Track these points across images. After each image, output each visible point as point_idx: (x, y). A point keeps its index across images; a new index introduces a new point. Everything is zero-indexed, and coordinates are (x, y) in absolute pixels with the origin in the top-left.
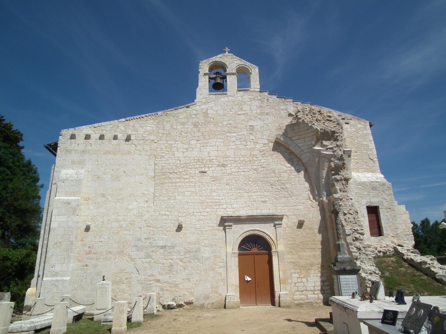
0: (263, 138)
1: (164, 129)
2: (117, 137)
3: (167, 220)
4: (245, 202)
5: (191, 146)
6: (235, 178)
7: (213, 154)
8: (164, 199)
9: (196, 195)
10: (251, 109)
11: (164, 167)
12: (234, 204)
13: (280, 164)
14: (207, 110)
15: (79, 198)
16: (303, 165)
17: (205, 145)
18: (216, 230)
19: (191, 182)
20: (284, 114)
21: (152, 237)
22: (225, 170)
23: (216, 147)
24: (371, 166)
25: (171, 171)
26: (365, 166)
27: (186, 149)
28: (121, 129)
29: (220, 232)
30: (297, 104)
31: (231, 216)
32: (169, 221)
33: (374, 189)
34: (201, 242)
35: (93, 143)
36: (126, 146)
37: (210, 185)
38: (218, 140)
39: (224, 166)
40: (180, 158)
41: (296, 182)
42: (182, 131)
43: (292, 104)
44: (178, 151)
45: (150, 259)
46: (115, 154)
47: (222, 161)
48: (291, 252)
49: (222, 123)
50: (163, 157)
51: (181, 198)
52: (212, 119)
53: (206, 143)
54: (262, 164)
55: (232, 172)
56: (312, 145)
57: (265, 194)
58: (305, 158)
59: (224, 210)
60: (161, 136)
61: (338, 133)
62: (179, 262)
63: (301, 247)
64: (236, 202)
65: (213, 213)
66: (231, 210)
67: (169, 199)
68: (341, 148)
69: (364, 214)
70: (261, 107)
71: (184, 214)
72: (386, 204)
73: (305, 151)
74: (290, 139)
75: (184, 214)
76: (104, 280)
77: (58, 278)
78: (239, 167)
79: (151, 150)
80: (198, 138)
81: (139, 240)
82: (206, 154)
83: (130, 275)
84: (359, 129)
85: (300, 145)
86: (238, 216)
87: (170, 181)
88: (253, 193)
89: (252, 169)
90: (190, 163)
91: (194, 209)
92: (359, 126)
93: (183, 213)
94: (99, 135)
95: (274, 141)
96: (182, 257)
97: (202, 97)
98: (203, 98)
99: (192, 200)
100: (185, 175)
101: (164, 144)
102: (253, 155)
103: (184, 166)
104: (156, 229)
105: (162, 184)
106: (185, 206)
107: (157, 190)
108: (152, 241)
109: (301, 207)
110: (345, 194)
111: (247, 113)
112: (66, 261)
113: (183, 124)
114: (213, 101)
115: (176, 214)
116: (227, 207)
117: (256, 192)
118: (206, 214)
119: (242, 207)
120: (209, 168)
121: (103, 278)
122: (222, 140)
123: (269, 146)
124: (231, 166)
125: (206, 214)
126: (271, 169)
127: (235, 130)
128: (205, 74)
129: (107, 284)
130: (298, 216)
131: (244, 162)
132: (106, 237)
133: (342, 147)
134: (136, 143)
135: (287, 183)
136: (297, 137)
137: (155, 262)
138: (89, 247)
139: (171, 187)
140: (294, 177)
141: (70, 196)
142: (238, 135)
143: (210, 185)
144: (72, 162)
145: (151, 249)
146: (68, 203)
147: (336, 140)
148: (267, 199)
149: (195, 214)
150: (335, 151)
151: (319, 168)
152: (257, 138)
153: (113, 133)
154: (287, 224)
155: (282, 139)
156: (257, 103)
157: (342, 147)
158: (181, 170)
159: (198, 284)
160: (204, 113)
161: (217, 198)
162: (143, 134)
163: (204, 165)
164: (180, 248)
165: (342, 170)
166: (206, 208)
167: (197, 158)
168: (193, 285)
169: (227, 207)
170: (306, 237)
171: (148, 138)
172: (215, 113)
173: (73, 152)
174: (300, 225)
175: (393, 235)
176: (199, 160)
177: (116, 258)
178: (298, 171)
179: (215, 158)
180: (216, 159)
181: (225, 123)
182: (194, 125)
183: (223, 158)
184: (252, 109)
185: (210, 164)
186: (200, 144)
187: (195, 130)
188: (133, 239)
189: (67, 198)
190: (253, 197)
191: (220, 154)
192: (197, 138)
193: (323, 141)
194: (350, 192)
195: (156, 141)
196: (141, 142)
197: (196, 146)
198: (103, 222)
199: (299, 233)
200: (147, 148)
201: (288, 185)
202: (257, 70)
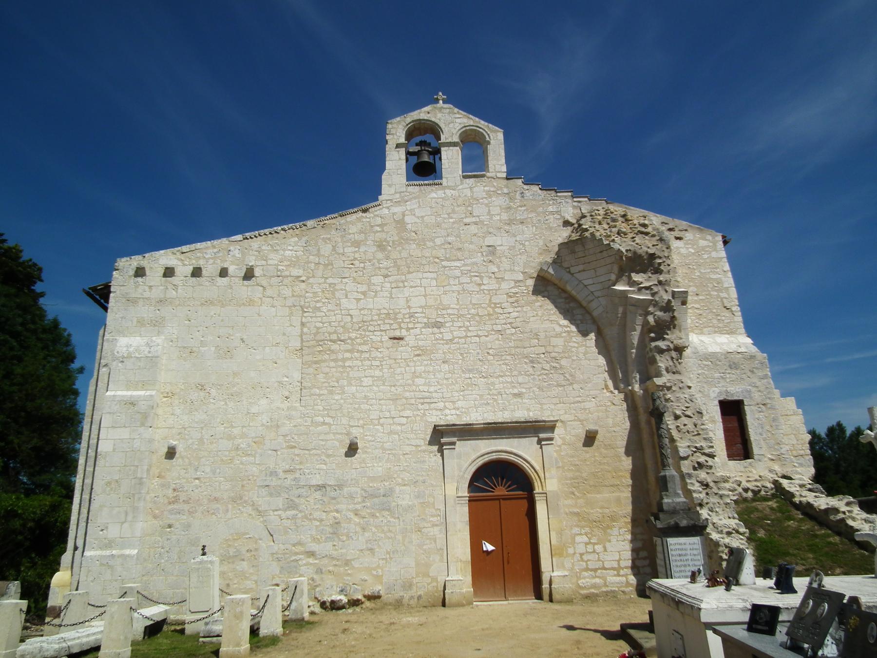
1: (318, 255)
4: (481, 396)
5: (372, 287)
7: (417, 302)
8: (322, 392)
9: (384, 385)
12: (459, 400)
13: (547, 319)
14: (404, 215)
15: (154, 393)
17: (401, 285)
19: (374, 359)
20: (555, 222)
21: (298, 467)
22: (441, 333)
25: (334, 337)
26: (715, 321)
27: (364, 293)
28: (234, 256)
30: (579, 202)
31: (454, 425)
32: (331, 436)
33: (734, 366)
34: (395, 476)
36: (244, 290)
37: (411, 364)
38: (425, 275)
39: (438, 325)
40: (351, 312)
41: (581, 356)
42: (355, 259)
43: (570, 201)
44: (346, 297)
46: (223, 306)
48: (573, 493)
50: (319, 309)
51: (354, 391)
52: (413, 234)
53: (403, 282)
54: (513, 321)
55: (454, 338)
57: (520, 379)
58: (598, 308)
59: (439, 413)
60: (313, 268)
61: (660, 258)
62: (352, 515)
63: (592, 483)
64: (463, 396)
65: (418, 418)
66: (454, 412)
67: (331, 393)
68: (667, 288)
70: (509, 208)
71: (361, 422)
72: (757, 396)
73: (597, 294)
76: (204, 554)
77: (114, 552)
78: (467, 327)
79: (293, 296)
81: (274, 473)
82: (402, 302)
83: (256, 543)
84: (703, 250)
85: (586, 282)
86: (467, 425)
87: (333, 357)
88: (497, 378)
89: (493, 330)
90: (372, 320)
92: (702, 243)
93: (358, 419)
94: (191, 268)
95: (535, 275)
97: (392, 191)
98: (396, 193)
99: (375, 393)
101: (320, 284)
103: (360, 328)
104: (307, 452)
105: (316, 363)
108: (297, 475)
109: (591, 405)
110: (677, 376)
111: (482, 222)
112: (130, 518)
113: (357, 244)
114: (415, 198)
115: (345, 421)
117: (502, 376)
118: (404, 420)
119: (476, 407)
120: (408, 329)
121: (203, 549)
122: (434, 275)
123: (525, 286)
126: (531, 332)
127: (459, 254)
129: (211, 562)
131: (477, 318)
132: (208, 469)
133: (669, 285)
135: (562, 358)
136: (581, 267)
137: (306, 517)
138: (174, 490)
139: (334, 370)
140: (576, 345)
141: (136, 389)
142: (464, 265)
143: (411, 364)
145: (297, 492)
146: (133, 404)
147: (658, 271)
148: (524, 390)
149: (382, 421)
150: (656, 293)
151: (624, 329)
154: (563, 439)
155: (551, 271)
156: (501, 201)
157: (669, 285)
158: (353, 335)
160: (397, 222)
161: (426, 388)
162: (278, 265)
163: (399, 324)
164: (353, 489)
165: (670, 330)
168: (381, 562)
170: (600, 463)
171: (287, 273)
173: (141, 303)
174: (590, 439)
176: (389, 314)
177: (227, 511)
179: (420, 310)
180: (422, 313)
181: (438, 241)
182: (379, 246)
183: (437, 309)
184: (492, 213)
185: (410, 322)
187: (380, 255)
188: (261, 471)
189: (129, 393)
190: (497, 387)
191: (431, 302)
193: (633, 275)
195: (304, 278)
196: (275, 280)
198: (201, 440)
199: (588, 455)
200: (287, 292)
201: (564, 362)
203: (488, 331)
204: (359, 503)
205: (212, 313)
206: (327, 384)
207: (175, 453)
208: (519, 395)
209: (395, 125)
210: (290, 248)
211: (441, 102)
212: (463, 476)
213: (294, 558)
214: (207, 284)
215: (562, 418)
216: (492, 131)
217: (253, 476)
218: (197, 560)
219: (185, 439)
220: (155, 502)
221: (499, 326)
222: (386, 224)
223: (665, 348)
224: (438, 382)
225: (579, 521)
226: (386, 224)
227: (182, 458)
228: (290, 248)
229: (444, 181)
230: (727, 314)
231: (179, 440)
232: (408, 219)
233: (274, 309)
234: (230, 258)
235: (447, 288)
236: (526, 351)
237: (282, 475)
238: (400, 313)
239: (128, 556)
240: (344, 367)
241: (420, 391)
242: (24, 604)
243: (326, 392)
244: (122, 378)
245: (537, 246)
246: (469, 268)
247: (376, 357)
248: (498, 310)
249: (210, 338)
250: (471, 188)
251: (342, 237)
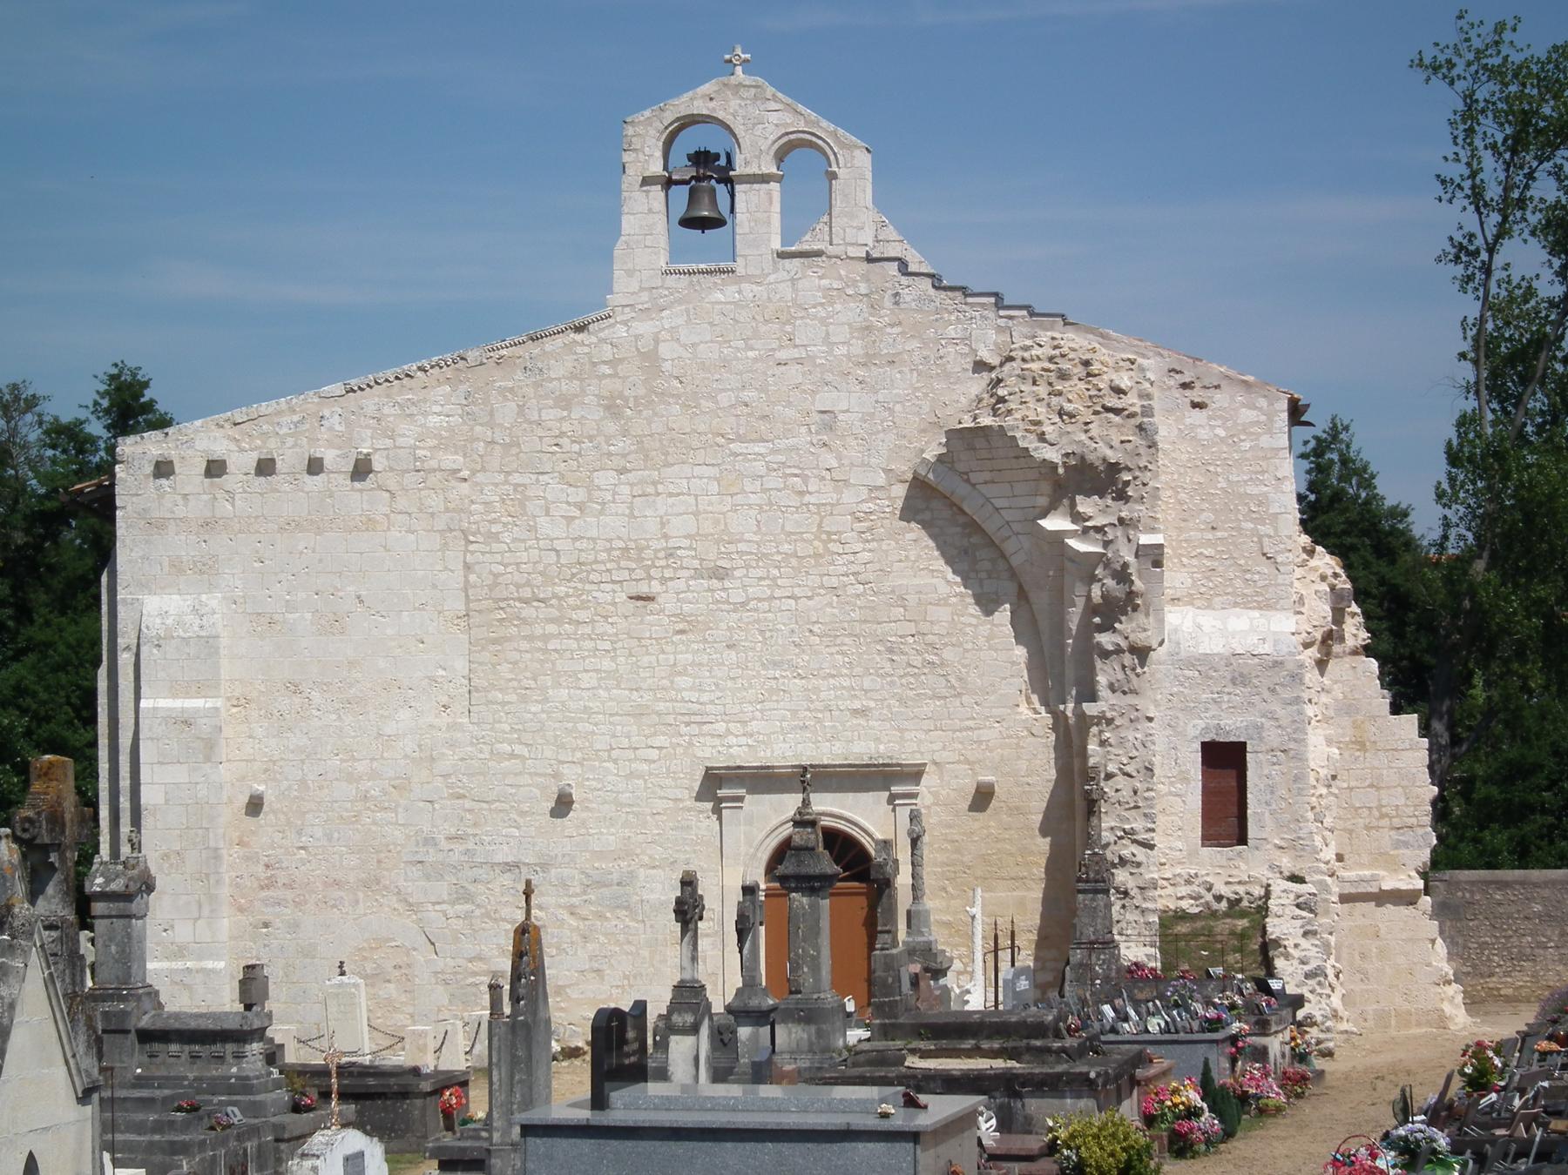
0: (868, 465)
1: (491, 425)
2: (322, 465)
3: (521, 773)
4: (794, 712)
5: (596, 494)
6: (758, 621)
7: (681, 526)
8: (507, 698)
9: (618, 686)
10: (826, 339)
11: (500, 580)
12: (754, 719)
13: (923, 570)
14: (657, 341)
15: (219, 703)
16: (1013, 574)
17: (651, 490)
18: (689, 810)
19: (601, 637)
20: (957, 361)
21: (470, 831)
22: (724, 589)
23: (691, 500)
24: (1260, 583)
25: (526, 593)
26: (1238, 583)
27: (580, 507)
28: (331, 429)
29: (702, 820)
30: (1011, 318)
31: (739, 767)
32: (526, 779)
33: (1240, 679)
34: (638, 851)
35: (238, 488)
36: (356, 498)
37: (669, 648)
38: (698, 471)
39: (719, 574)
40: (557, 545)
42: (562, 435)
43: (991, 315)
44: (547, 514)
45: (468, 907)
46: (319, 531)
47: (712, 556)
48: (944, 889)
49: (713, 398)
50: (495, 537)
51: (565, 697)
52: (676, 383)
53: (654, 483)
54: (861, 569)
55: (749, 600)
56: (1037, 511)
57: (867, 683)
58: (1018, 551)
59: (717, 742)
60: (481, 451)
61: (1130, 470)
62: (566, 916)
63: (979, 873)
64: (762, 711)
65: (680, 750)
66: (743, 740)
67: (524, 699)
69: (1188, 772)
70: (868, 328)
71: (579, 755)
72: (1273, 736)
73: (1015, 527)
74: (965, 477)
75: (579, 755)
76: (343, 974)
77: (189, 964)
78: (774, 579)
79: (447, 510)
80: (622, 462)
81: (430, 841)
82: (652, 526)
83: (408, 954)
84: (1244, 431)
85: (999, 503)
86: (762, 768)
87: (526, 631)
88: (824, 678)
89: (822, 586)
90: (596, 562)
91: (614, 736)
92: (1247, 415)
93: (574, 750)
94: (255, 456)
95: (909, 476)
96: (575, 900)
97: (635, 286)
98: (642, 289)
99: (603, 703)
100: (578, 608)
101: (496, 485)
102: (829, 533)
103: (574, 575)
104: (485, 806)
105: (495, 642)
106: (580, 726)
107: (480, 664)
108: (471, 846)
109: (990, 734)
110: (1130, 699)
111: (812, 358)
112: (206, 912)
113: (565, 402)
114: (680, 302)
115: (549, 752)
116: (728, 730)
117: (833, 676)
118: (654, 754)
119: (782, 731)
120: (663, 581)
121: (341, 967)
122: (713, 471)
123: (889, 498)
124: (746, 576)
125: (654, 754)
126: (893, 592)
127: (763, 427)
128: (647, 181)
129: (356, 986)
130: (977, 767)
131: (794, 562)
132: (319, 833)
134: (392, 482)
135: (946, 645)
136: (987, 476)
137: (487, 914)
138: (267, 866)
139: (529, 656)
141: (188, 696)
142: (774, 452)
143: (669, 648)
144: (172, 565)
145: (471, 874)
146: (186, 723)
147: (1122, 496)
148: (872, 704)
149: (614, 754)
152: (845, 462)
153: (308, 450)
154: (935, 795)
155: (931, 476)
156: (850, 312)
158: (561, 590)
159: (631, 986)
160: (643, 356)
161: (694, 696)
162: (416, 448)
163: (647, 569)
164: (566, 872)
165: (1126, 614)
166: (655, 734)
167: (621, 544)
168: (614, 991)
169: (728, 730)
170: (998, 840)
171: (433, 464)
172: (686, 355)
173: (172, 527)
174: (982, 798)
175: (1283, 844)
176: (627, 549)
177: (357, 902)
178: (987, 604)
179: (686, 543)
180: (690, 548)
181: (725, 399)
182: (607, 408)
183: (717, 542)
184: (833, 339)
185: (668, 566)
186: (632, 485)
187: (611, 427)
188: (408, 837)
189: (178, 703)
190: (823, 695)
191: (707, 527)
192: (618, 462)
193: (1078, 498)
194: (1150, 693)
195: (465, 473)
196: (410, 479)
197: (615, 493)
198: (303, 782)
199: (976, 825)
200: (435, 502)
201: (948, 654)
202: (864, 160)
203: (813, 589)
204: (577, 895)
205: (300, 548)
206: (515, 684)
207: (262, 805)
208: (862, 712)
209: (640, 129)
210: (436, 409)
211: (739, 70)
212: (755, 855)
213: (471, 980)
214: (286, 487)
215: (937, 758)
216: (843, 146)
217: (396, 845)
218: (334, 981)
219: (275, 780)
220: (237, 886)
221: (834, 579)
222: (621, 360)
223: (1111, 648)
224: (717, 685)
225: (951, 935)
226: (621, 360)
227: (274, 812)
228: (436, 409)
229: (740, 266)
230: (1266, 568)
231: (265, 782)
232: (665, 350)
233: (412, 537)
234: (324, 434)
235: (739, 499)
236: (879, 629)
237: (444, 845)
238: (648, 547)
239: (213, 971)
240: (545, 651)
241: (683, 700)
242: (1076, 920)
243: (514, 698)
244: (161, 675)
245: (919, 414)
246: (781, 458)
247: (605, 633)
248: (834, 547)
249: (302, 595)
250: (792, 280)
251: (538, 385)
